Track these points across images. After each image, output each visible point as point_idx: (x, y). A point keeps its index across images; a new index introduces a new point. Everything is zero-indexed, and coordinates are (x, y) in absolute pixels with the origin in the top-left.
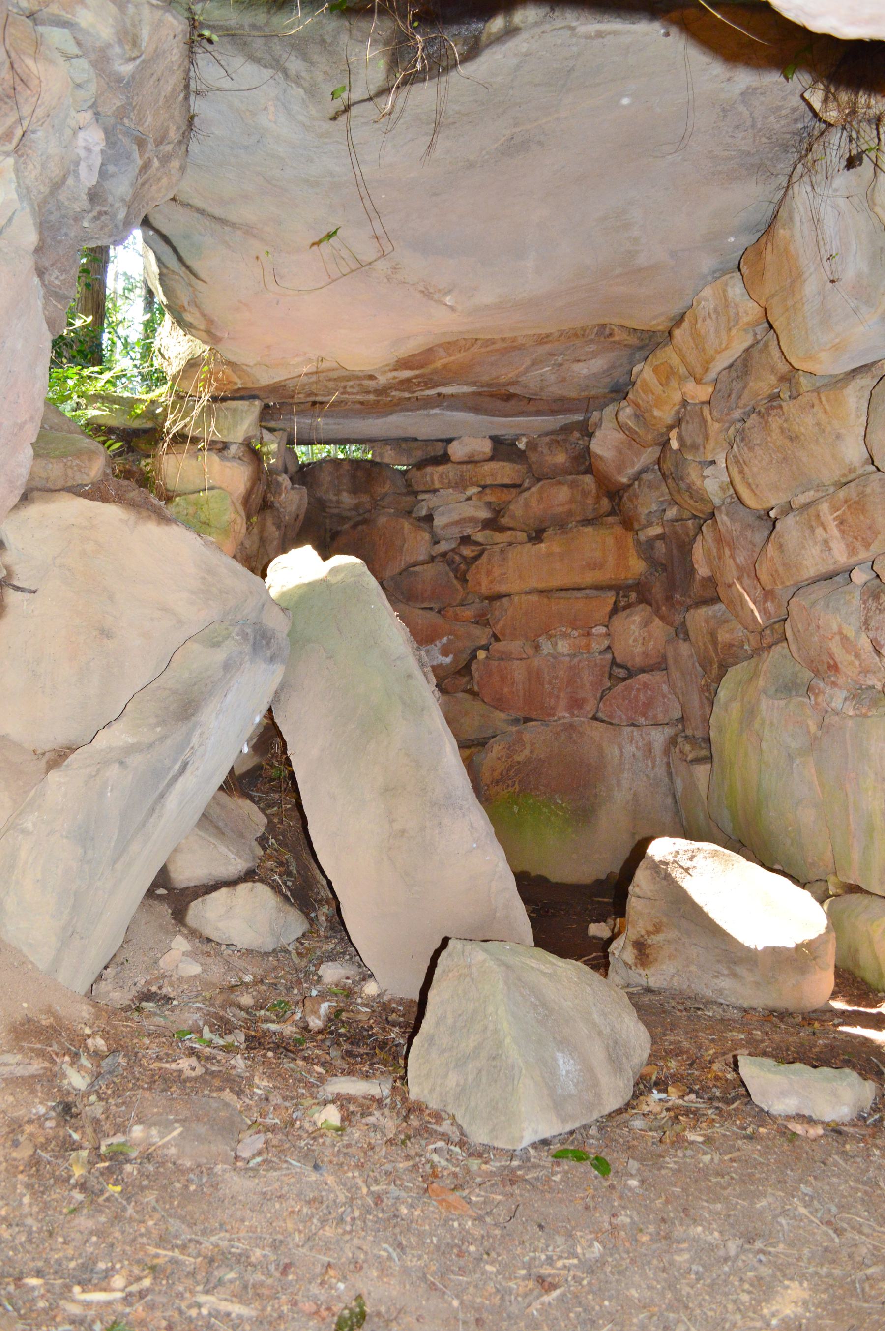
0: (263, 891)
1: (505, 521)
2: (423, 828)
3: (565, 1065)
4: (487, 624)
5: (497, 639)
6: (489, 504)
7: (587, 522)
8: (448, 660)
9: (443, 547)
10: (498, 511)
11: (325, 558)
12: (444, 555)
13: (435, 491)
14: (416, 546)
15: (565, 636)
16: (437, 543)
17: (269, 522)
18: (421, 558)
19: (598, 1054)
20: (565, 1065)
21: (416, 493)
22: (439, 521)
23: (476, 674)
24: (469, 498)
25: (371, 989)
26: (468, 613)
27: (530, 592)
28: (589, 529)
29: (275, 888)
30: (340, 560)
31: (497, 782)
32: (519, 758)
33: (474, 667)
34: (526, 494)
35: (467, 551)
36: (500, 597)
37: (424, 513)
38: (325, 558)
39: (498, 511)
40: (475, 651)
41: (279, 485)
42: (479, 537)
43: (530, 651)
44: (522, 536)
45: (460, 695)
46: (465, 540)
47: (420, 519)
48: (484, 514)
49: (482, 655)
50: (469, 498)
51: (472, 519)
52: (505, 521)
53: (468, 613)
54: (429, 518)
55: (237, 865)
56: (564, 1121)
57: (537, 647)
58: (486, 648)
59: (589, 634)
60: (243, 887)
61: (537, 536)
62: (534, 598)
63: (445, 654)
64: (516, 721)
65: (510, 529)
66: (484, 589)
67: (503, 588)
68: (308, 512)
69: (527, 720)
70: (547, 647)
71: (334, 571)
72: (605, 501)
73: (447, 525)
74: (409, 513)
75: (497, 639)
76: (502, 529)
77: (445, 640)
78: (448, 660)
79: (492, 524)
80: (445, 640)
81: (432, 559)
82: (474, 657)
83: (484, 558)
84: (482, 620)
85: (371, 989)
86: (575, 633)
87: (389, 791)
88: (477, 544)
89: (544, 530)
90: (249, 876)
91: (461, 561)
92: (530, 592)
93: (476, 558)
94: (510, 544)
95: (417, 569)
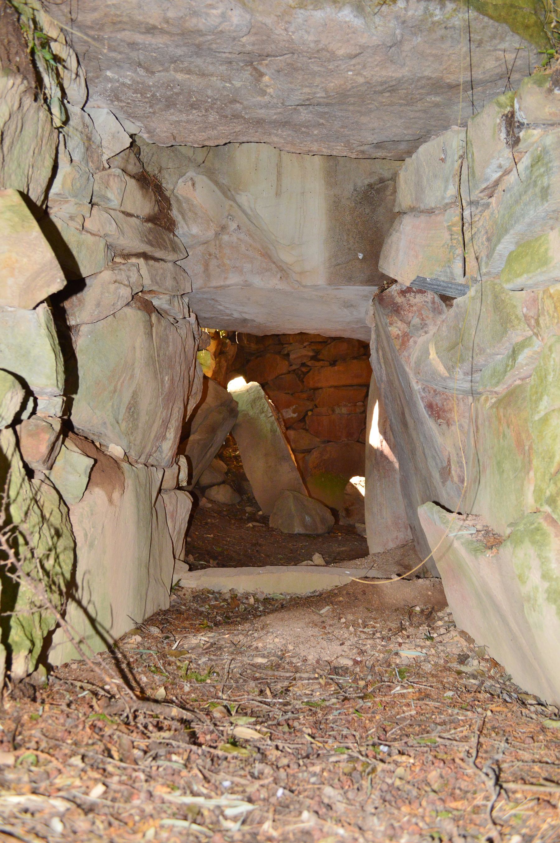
0: (228, 487)
1: (320, 357)
2: (276, 465)
3: (308, 518)
4: (312, 400)
5: (317, 407)
6: (313, 350)
7: (354, 358)
8: (295, 415)
9: (294, 367)
10: (317, 353)
11: (248, 382)
12: (294, 370)
13: (291, 344)
14: (283, 367)
15: (345, 406)
16: (291, 365)
17: (223, 360)
18: (285, 372)
19: (318, 519)
20: (308, 518)
21: (283, 344)
22: (292, 356)
23: (307, 422)
24: (305, 347)
25: (260, 513)
26: (304, 395)
27: (331, 387)
28: (355, 361)
29: (231, 486)
30: (251, 383)
31: (315, 468)
32: (325, 458)
33: (306, 418)
34: (329, 346)
35: (304, 369)
36: (318, 389)
37: (286, 352)
38: (248, 382)
39: (317, 353)
40: (307, 412)
41: (226, 344)
42: (309, 363)
43: (330, 412)
44: (327, 363)
45: (301, 431)
46: (303, 365)
47: (285, 355)
48: (311, 354)
49: (310, 413)
50: (305, 347)
51: (306, 356)
52: (320, 357)
53: (304, 395)
54: (288, 355)
55: (220, 479)
56: (306, 530)
57: (333, 411)
58: (312, 410)
59: (355, 405)
60: (222, 486)
61: (333, 363)
62: (332, 389)
63: (294, 413)
64: (324, 442)
65: (323, 360)
66: (311, 385)
67: (320, 385)
68: (237, 354)
69: (329, 442)
70: (337, 411)
71: (251, 388)
72: (362, 349)
73: (295, 359)
74: (280, 352)
75: (317, 407)
76: (319, 360)
77: (294, 407)
78: (295, 415)
79: (314, 358)
80: (294, 407)
81: (289, 372)
82: (307, 414)
83: (310, 373)
84: (310, 399)
85: (260, 513)
86: (349, 405)
87: (266, 455)
88: (308, 366)
89: (336, 361)
90: (223, 482)
91: (301, 373)
92: (331, 387)
93: (308, 372)
94: (322, 367)
95: (283, 376)
